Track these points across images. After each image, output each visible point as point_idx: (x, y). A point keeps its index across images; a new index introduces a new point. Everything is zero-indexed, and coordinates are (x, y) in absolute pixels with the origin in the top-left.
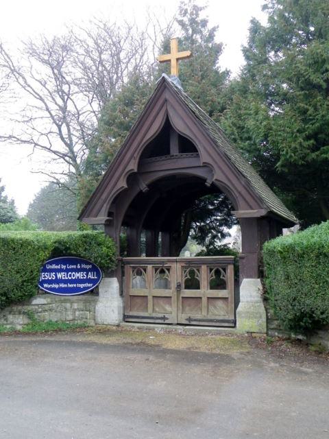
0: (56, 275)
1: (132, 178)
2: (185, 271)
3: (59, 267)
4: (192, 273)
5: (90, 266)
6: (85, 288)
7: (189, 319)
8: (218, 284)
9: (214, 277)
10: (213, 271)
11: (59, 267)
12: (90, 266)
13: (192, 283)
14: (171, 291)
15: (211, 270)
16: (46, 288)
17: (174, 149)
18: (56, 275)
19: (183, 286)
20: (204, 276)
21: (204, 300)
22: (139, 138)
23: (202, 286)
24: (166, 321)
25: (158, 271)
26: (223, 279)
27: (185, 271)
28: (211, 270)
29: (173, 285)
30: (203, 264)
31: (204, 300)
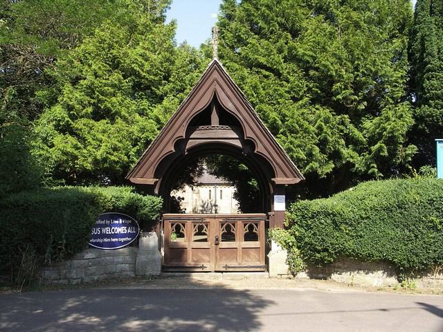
0: (101, 230)
1: (180, 143)
2: (195, 226)
3: (104, 222)
4: (228, 228)
5: (130, 221)
6: (125, 242)
7: (226, 267)
8: (251, 236)
9: (248, 231)
10: (247, 226)
11: (104, 222)
12: (130, 221)
13: (229, 236)
14: (209, 243)
15: (245, 225)
16: (92, 243)
17: (215, 118)
18: (101, 230)
19: (220, 239)
20: (240, 231)
21: (240, 250)
22: (279, 161)
23: (237, 237)
24: (205, 270)
25: (247, 226)
26: (255, 233)
27: (195, 226)
28: (245, 225)
29: (212, 238)
30: (240, 220)
31: (240, 250)
